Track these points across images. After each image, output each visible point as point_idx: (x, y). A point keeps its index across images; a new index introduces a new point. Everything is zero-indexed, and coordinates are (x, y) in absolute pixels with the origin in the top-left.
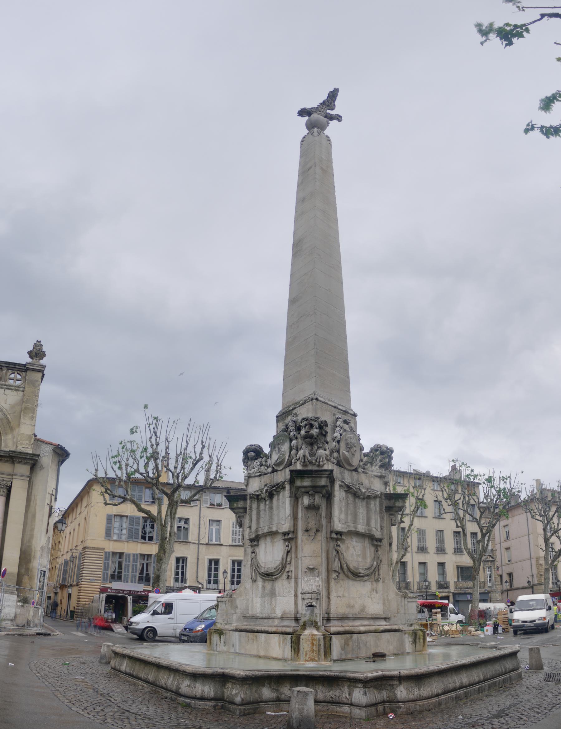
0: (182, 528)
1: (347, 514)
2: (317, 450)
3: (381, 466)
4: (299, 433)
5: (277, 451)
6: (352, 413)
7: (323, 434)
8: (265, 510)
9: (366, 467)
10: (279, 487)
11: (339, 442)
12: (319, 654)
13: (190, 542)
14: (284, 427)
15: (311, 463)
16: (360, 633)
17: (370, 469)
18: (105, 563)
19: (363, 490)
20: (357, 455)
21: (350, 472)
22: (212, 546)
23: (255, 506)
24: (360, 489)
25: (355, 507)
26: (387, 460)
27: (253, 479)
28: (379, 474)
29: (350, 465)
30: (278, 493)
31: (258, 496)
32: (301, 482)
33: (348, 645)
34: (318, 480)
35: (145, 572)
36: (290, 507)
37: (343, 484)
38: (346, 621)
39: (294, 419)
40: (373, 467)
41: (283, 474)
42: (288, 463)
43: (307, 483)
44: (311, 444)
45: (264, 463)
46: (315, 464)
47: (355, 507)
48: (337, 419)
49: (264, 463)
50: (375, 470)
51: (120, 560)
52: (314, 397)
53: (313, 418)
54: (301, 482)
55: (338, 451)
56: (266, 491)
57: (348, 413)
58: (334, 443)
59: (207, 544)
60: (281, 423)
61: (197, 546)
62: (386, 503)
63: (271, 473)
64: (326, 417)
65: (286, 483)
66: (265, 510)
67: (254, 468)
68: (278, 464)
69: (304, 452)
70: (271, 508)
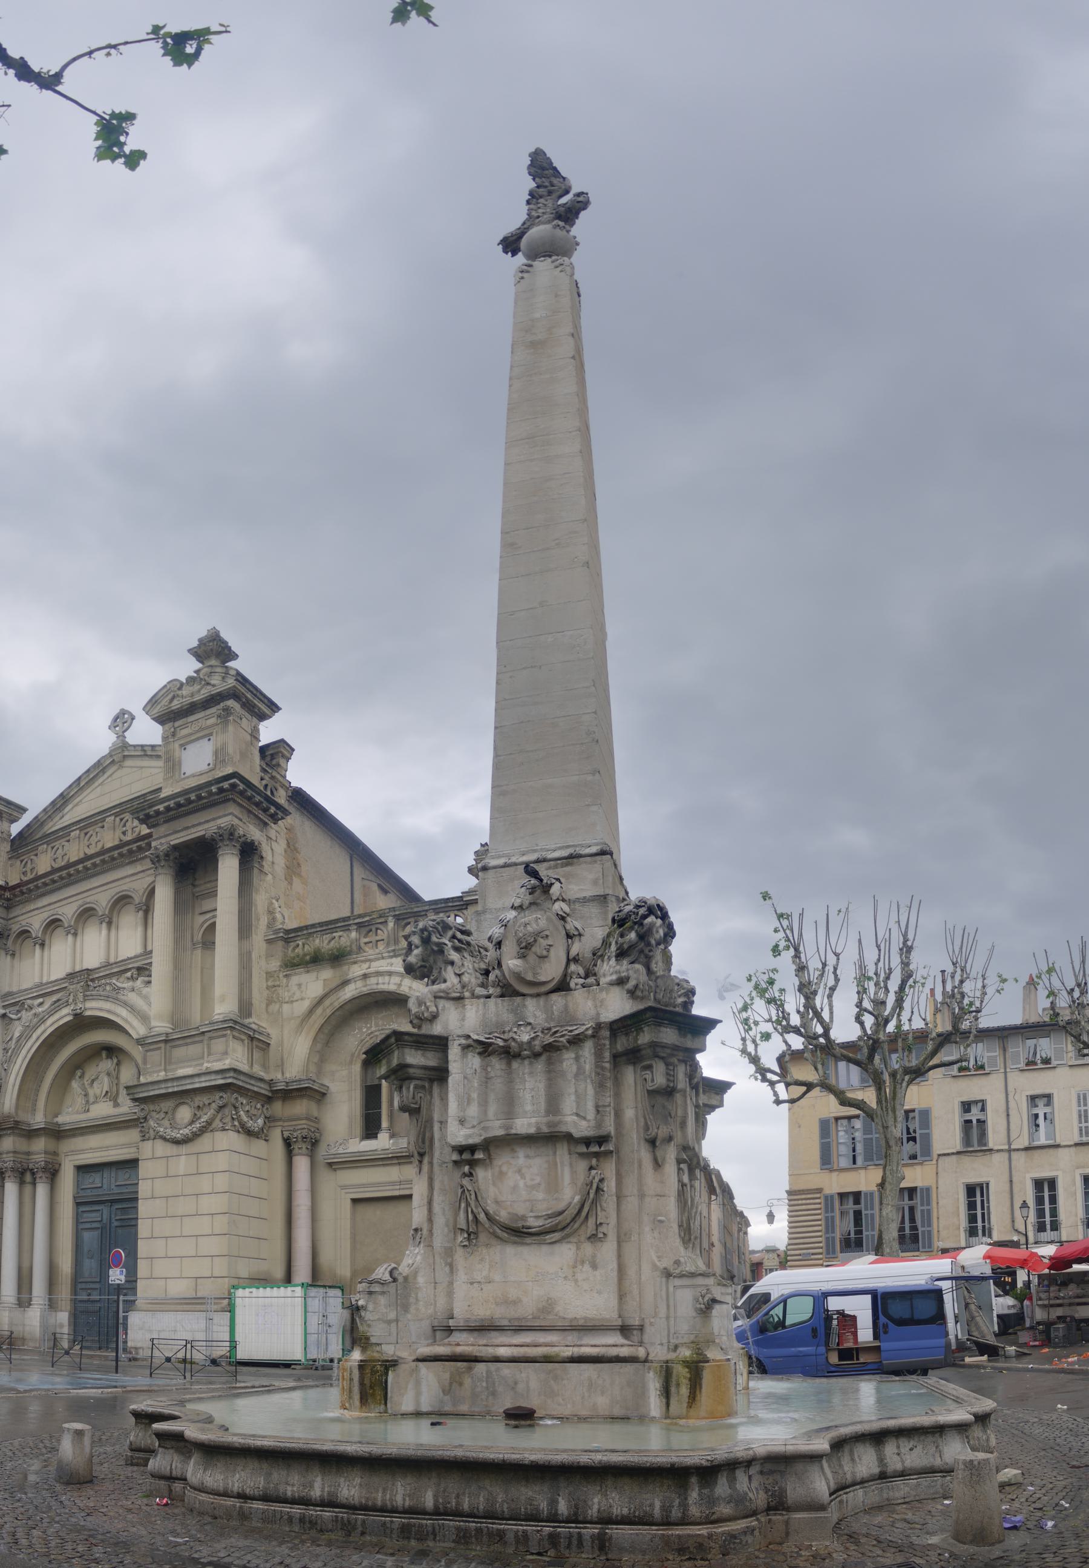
0: (975, 1122)
1: (484, 1103)
12: (350, 1398)
13: (991, 1150)
16: (497, 1360)
18: (827, 1218)
22: (1039, 1151)
25: (510, 1081)
28: (614, 977)
33: (461, 1384)
35: (907, 1225)
37: (470, 1042)
38: (494, 1334)
51: (857, 1207)
57: (581, 856)
59: (1026, 1149)
61: (1006, 1155)
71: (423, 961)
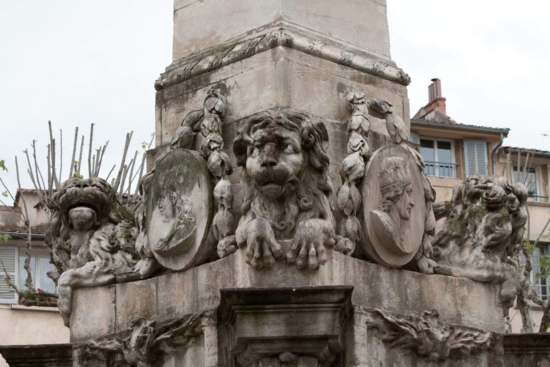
2: (296, 219)
3: (490, 249)
4: (243, 164)
6: (393, 73)
7: (315, 166)
9: (444, 252)
10: (181, 333)
11: (359, 182)
14: (186, 128)
15: (280, 259)
17: (457, 258)
19: (440, 335)
20: (417, 219)
21: (396, 275)
24: (429, 333)
26: (509, 227)
27: (90, 292)
28: (485, 274)
29: (397, 252)
30: (179, 351)
31: (110, 354)
32: (257, 325)
34: (307, 318)
39: (219, 104)
40: (466, 251)
41: (189, 285)
42: (205, 251)
43: (273, 328)
44: (280, 201)
45: (123, 242)
46: (294, 263)
48: (350, 108)
49: (123, 242)
50: (473, 260)
52: (281, 37)
53: (284, 120)
54: (257, 325)
55: (359, 212)
56: (141, 342)
57: (382, 76)
58: (345, 188)
60: (172, 110)
64: (317, 105)
65: (205, 321)
67: (90, 259)
69: (261, 227)
71: (298, 176)
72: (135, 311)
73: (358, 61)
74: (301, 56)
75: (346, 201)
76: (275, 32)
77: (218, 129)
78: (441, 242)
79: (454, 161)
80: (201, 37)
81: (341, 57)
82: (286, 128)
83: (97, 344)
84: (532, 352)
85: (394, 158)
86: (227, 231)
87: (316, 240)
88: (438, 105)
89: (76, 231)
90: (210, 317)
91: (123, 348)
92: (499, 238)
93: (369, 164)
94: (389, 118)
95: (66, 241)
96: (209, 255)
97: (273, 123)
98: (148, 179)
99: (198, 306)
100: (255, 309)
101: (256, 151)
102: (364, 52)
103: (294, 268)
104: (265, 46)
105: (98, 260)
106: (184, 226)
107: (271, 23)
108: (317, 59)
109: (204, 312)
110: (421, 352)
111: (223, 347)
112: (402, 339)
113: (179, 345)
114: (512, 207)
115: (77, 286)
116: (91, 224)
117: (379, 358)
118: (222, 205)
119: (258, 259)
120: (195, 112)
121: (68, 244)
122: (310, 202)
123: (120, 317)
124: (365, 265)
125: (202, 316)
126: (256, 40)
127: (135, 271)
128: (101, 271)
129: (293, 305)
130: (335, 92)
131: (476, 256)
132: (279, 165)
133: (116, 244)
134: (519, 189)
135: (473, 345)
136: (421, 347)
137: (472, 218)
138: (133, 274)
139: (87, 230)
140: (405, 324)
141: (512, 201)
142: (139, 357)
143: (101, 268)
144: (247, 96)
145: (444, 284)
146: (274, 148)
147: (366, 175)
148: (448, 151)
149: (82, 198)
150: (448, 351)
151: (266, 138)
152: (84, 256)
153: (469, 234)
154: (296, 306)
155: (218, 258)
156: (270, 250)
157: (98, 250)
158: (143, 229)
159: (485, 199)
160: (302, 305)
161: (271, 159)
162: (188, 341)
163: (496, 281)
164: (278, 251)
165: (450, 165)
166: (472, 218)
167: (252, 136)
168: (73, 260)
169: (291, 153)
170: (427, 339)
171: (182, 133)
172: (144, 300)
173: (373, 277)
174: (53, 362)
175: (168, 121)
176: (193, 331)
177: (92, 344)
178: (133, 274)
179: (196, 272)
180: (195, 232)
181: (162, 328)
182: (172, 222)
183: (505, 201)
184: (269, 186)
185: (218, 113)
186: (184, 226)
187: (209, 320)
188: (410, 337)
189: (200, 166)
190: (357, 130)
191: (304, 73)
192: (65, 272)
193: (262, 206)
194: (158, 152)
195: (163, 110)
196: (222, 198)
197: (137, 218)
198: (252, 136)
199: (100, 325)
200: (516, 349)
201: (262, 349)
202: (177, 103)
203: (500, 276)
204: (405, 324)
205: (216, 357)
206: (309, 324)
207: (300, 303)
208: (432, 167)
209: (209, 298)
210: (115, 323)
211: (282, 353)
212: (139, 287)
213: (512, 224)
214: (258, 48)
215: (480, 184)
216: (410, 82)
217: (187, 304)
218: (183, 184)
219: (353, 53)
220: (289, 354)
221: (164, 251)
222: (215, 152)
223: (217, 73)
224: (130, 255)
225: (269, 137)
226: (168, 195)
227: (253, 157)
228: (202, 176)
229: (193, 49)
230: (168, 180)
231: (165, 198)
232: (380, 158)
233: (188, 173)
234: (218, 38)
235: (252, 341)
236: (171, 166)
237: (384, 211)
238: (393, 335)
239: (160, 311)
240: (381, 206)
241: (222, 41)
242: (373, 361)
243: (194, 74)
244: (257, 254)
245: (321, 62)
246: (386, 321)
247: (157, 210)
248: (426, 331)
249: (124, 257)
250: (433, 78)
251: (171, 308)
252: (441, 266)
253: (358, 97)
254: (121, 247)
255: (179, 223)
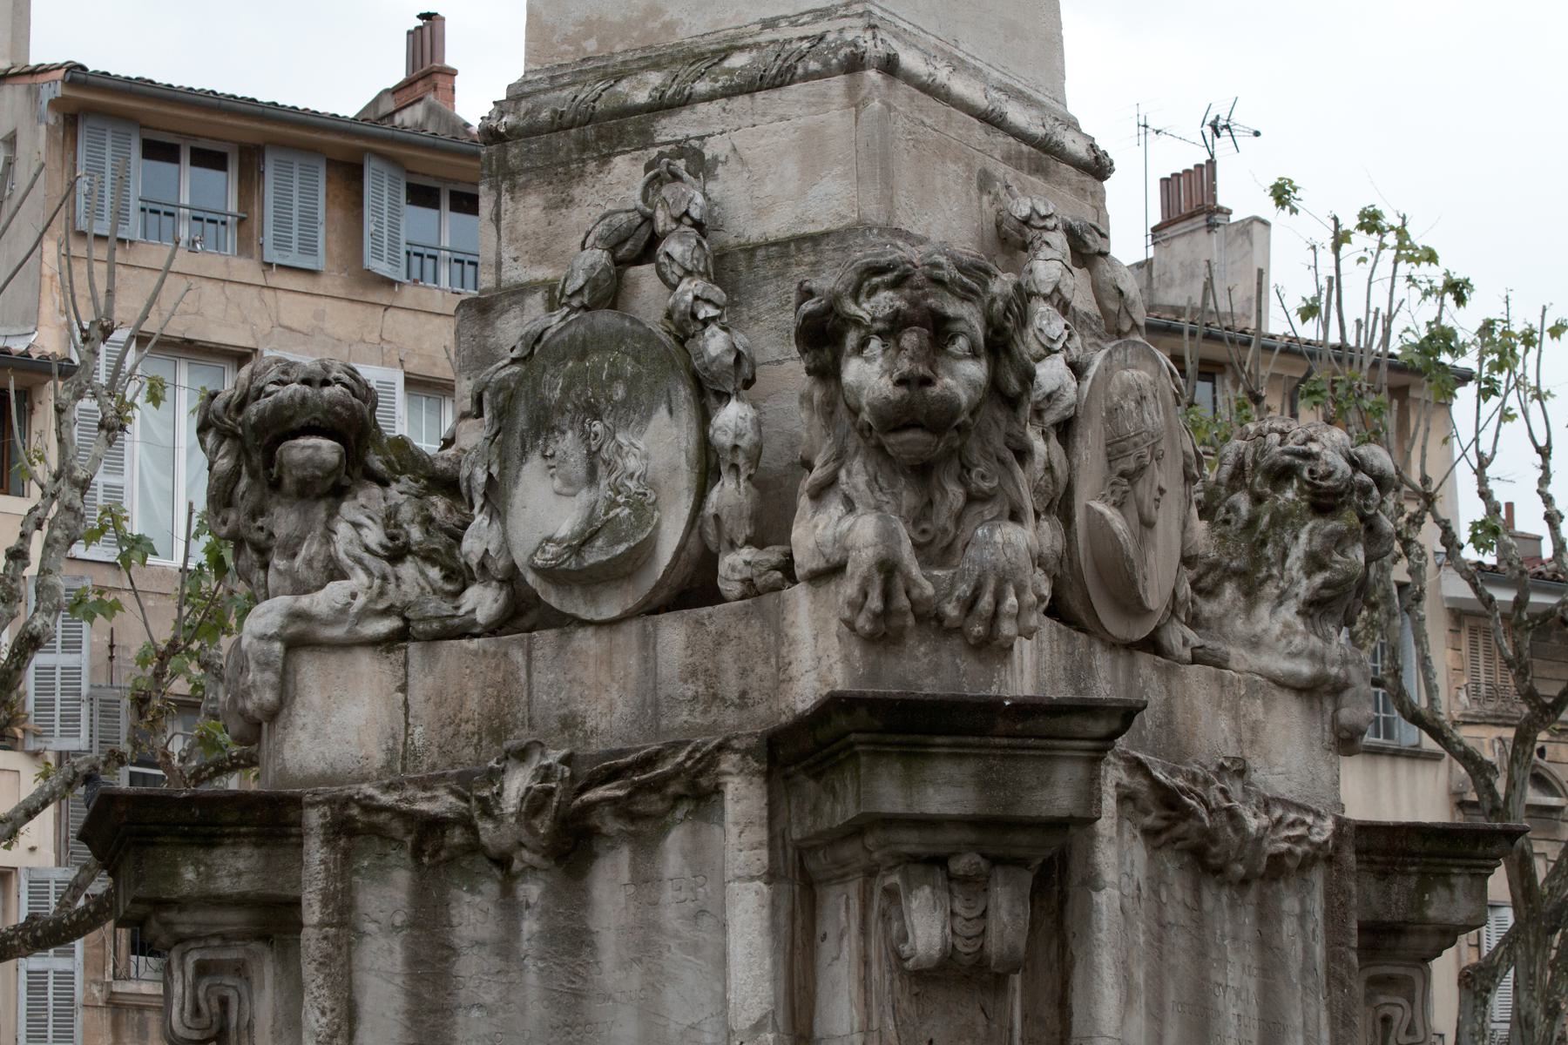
2: (959, 518)
3: (1317, 608)
5: (576, 463)
6: (1079, 149)
8: (506, 948)
9: (1208, 608)
15: (929, 618)
17: (1239, 625)
19: (1254, 823)
23: (386, 898)
24: (1232, 815)
25: (1201, 953)
27: (333, 660)
28: (1305, 669)
29: (1132, 605)
31: (431, 826)
32: (909, 783)
36: (774, 952)
40: (1263, 610)
41: (631, 662)
44: (922, 472)
45: (416, 533)
46: (958, 630)
47: (1201, 953)
49: (416, 533)
52: (873, 48)
53: (949, 272)
56: (534, 803)
62: (1368, 897)
63: (496, 628)
65: (728, 762)
66: (506, 948)
67: (335, 572)
68: (578, 570)
69: (887, 535)
70: (572, 940)
72: (464, 715)
73: (1017, 115)
74: (912, 98)
75: (1039, 476)
76: (855, 31)
77: (706, 267)
78: (1202, 585)
79: (233, 207)
80: (617, 18)
81: (986, 103)
82: (953, 293)
83: (387, 799)
84: (1414, 869)
85: (1135, 373)
86: (748, 532)
87: (1020, 576)
88: (435, 88)
89: (286, 496)
90: (746, 752)
91: (476, 814)
92: (1340, 584)
93: (1086, 385)
94: (1101, 267)
95: (254, 520)
96: (694, 587)
97: (918, 278)
98: (503, 380)
99: (657, 715)
100: (907, 744)
101: (875, 344)
102: (1021, 92)
103: (956, 642)
104: (826, 64)
105: (359, 579)
106: (627, 511)
107: (836, 8)
108: (941, 107)
109: (728, 740)
110: (1212, 861)
111: (778, 829)
112: (1182, 828)
113: (645, 817)
114: (1367, 506)
115: (300, 640)
116: (331, 481)
117: (1136, 874)
118: (735, 467)
119: (877, 617)
120: (622, 216)
121: (261, 529)
122: (992, 479)
123: (419, 730)
124: (1069, 635)
125: (721, 748)
126: (795, 45)
127: (462, 611)
128: (372, 606)
129: (997, 740)
130: (974, 193)
131: (1287, 625)
132: (939, 384)
133: (402, 540)
134: (1376, 463)
135: (1306, 847)
136: (1214, 850)
137: (1278, 530)
138: (456, 620)
139: (318, 498)
140: (1189, 792)
141: (1365, 491)
142: (524, 840)
143: (370, 601)
144: (769, 188)
145: (1215, 690)
146: (926, 343)
147: (1080, 412)
148: (220, 175)
149: (319, 415)
150: (1265, 860)
151: (905, 316)
152: (317, 565)
153: (1269, 568)
154: (1005, 741)
155: (715, 597)
156: (908, 593)
157: (359, 552)
158: (482, 507)
159: (1308, 483)
160: (1019, 741)
161: (922, 370)
162: (673, 808)
163: (1328, 688)
164: (928, 599)
165: (223, 218)
166: (1278, 530)
167: (865, 305)
168: (279, 572)
169: (965, 357)
170: (1229, 829)
171: (592, 267)
172: (489, 690)
173: (1081, 668)
174: (246, 835)
175: (521, 228)
176: (693, 785)
177: (371, 798)
178: (456, 620)
179: (650, 628)
180: (657, 527)
181: (599, 771)
182: (585, 496)
183: (1352, 493)
184: (908, 436)
185: (698, 225)
186: (627, 511)
187: (743, 758)
188: (1197, 824)
189: (672, 360)
190: (1047, 298)
191: (917, 140)
192: (266, 604)
193: (873, 481)
194: (499, 307)
195: (506, 197)
196: (735, 447)
197: (469, 479)
198: (865, 305)
199: (362, 745)
200: (1378, 859)
201: (910, 842)
202: (550, 183)
203: (1337, 677)
204: (1189, 792)
205: (764, 854)
206: (1032, 788)
207: (1014, 736)
208: (170, 219)
209: (695, 698)
210: (405, 744)
211: (956, 854)
212: (476, 654)
213: (1365, 550)
214: (806, 69)
215: (1291, 445)
216: (1112, 171)
217: (621, 709)
218: (624, 403)
219: (1006, 93)
220: (978, 858)
221: (567, 571)
222: (713, 328)
223: (675, 119)
224: (437, 569)
225: (911, 311)
226: (577, 426)
227: (867, 360)
228: (680, 387)
229: (591, 46)
230: (579, 388)
231: (563, 433)
232: (1107, 369)
233: (637, 377)
234: (669, 27)
235: (891, 822)
236: (583, 355)
237: (1114, 504)
238: (1165, 818)
239: (537, 720)
240: (1107, 491)
241: (683, 35)
242: (1125, 879)
243: (603, 113)
244: (875, 603)
245: (948, 114)
246: (1155, 783)
247: (535, 463)
248: (1229, 809)
249: (422, 573)
250: (425, 11)
251: (573, 715)
252: (1210, 644)
253: (1043, 212)
254: (414, 548)
255: (613, 504)
